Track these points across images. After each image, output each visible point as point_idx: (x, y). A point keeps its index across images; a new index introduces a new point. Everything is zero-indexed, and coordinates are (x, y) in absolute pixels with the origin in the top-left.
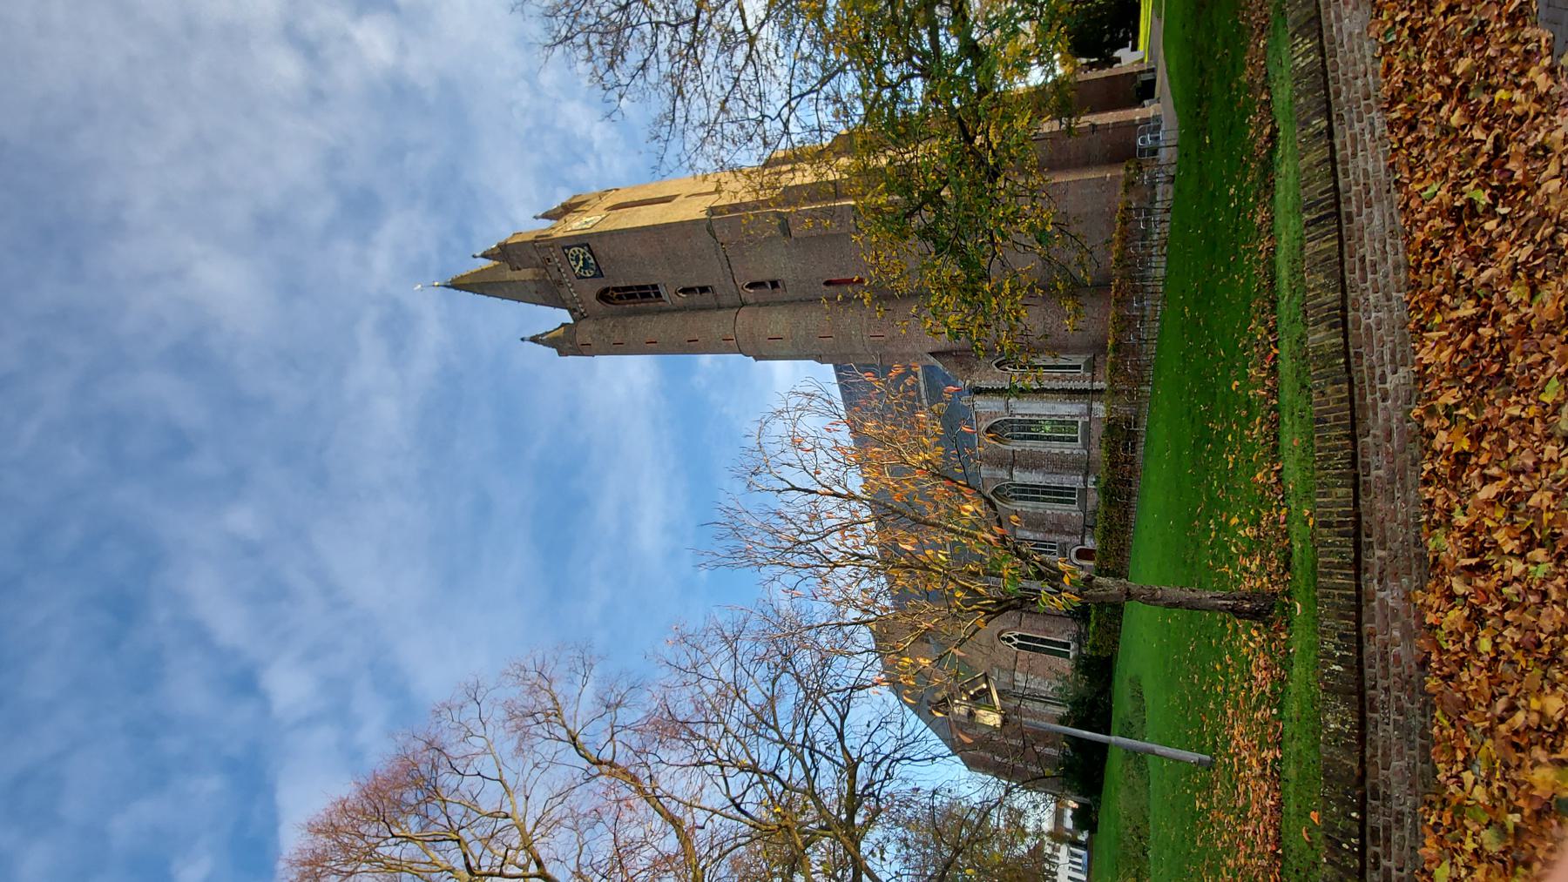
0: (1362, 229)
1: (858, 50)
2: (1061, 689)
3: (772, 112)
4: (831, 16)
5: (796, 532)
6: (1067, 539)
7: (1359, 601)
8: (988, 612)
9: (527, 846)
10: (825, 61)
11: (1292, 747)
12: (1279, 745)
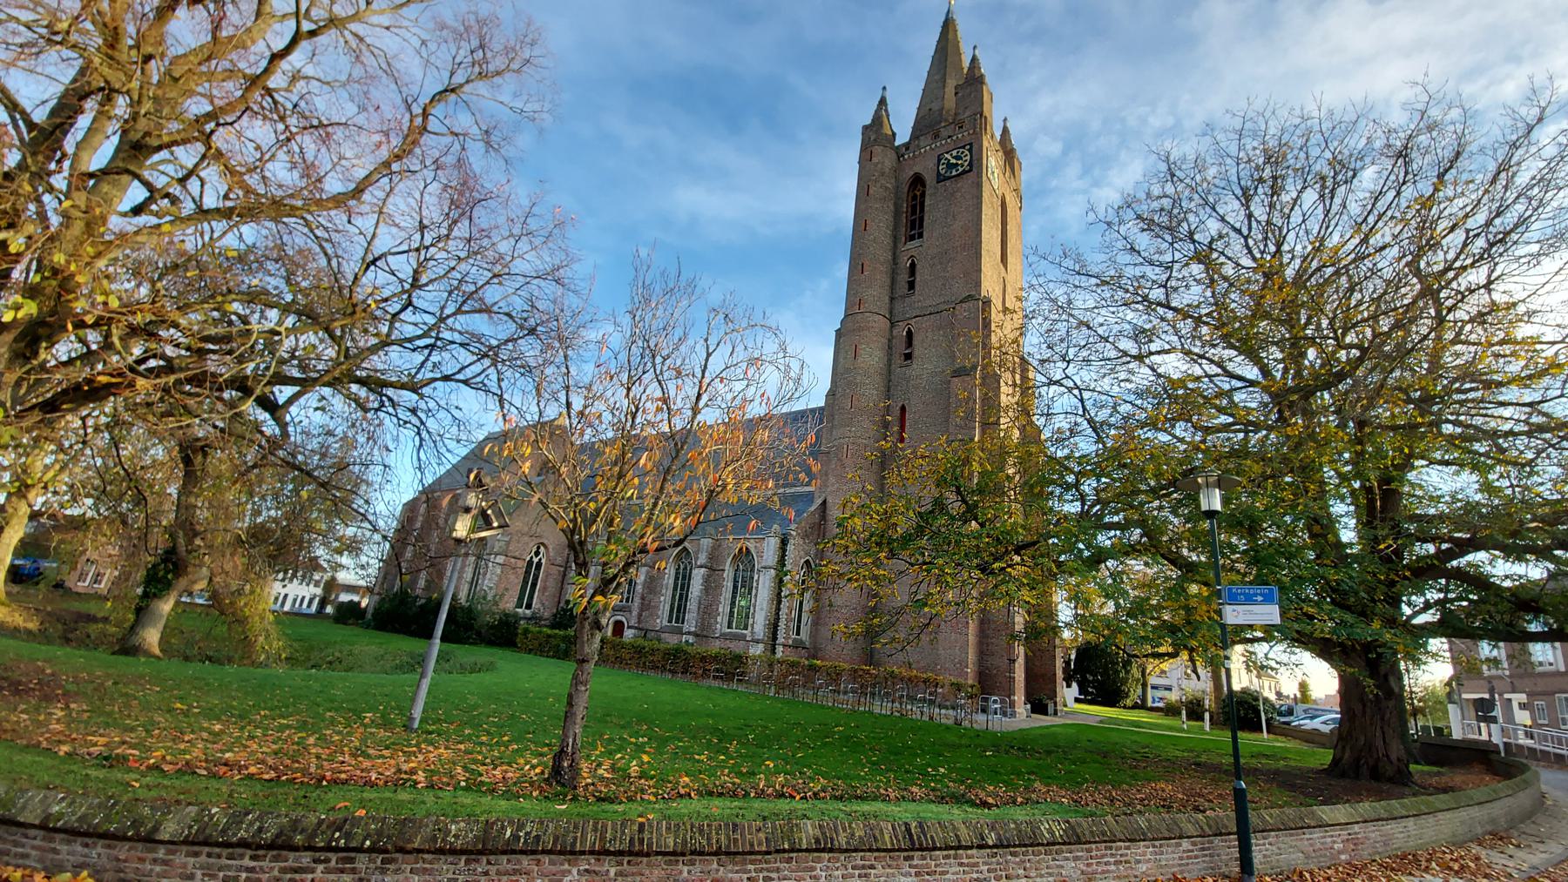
0: (898, 867)
1: (1112, 458)
2: (484, 598)
3: (1071, 371)
4: (1149, 434)
5: (665, 353)
6: (635, 613)
7: (571, 853)
8: (573, 532)
9: (333, 22)
10: (1110, 426)
11: (429, 797)
12: (431, 786)
